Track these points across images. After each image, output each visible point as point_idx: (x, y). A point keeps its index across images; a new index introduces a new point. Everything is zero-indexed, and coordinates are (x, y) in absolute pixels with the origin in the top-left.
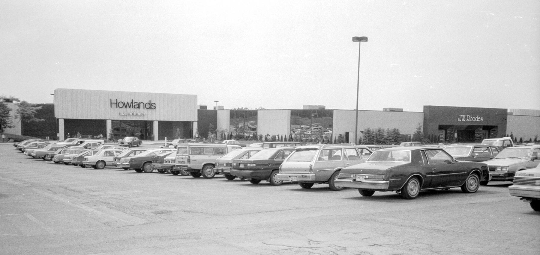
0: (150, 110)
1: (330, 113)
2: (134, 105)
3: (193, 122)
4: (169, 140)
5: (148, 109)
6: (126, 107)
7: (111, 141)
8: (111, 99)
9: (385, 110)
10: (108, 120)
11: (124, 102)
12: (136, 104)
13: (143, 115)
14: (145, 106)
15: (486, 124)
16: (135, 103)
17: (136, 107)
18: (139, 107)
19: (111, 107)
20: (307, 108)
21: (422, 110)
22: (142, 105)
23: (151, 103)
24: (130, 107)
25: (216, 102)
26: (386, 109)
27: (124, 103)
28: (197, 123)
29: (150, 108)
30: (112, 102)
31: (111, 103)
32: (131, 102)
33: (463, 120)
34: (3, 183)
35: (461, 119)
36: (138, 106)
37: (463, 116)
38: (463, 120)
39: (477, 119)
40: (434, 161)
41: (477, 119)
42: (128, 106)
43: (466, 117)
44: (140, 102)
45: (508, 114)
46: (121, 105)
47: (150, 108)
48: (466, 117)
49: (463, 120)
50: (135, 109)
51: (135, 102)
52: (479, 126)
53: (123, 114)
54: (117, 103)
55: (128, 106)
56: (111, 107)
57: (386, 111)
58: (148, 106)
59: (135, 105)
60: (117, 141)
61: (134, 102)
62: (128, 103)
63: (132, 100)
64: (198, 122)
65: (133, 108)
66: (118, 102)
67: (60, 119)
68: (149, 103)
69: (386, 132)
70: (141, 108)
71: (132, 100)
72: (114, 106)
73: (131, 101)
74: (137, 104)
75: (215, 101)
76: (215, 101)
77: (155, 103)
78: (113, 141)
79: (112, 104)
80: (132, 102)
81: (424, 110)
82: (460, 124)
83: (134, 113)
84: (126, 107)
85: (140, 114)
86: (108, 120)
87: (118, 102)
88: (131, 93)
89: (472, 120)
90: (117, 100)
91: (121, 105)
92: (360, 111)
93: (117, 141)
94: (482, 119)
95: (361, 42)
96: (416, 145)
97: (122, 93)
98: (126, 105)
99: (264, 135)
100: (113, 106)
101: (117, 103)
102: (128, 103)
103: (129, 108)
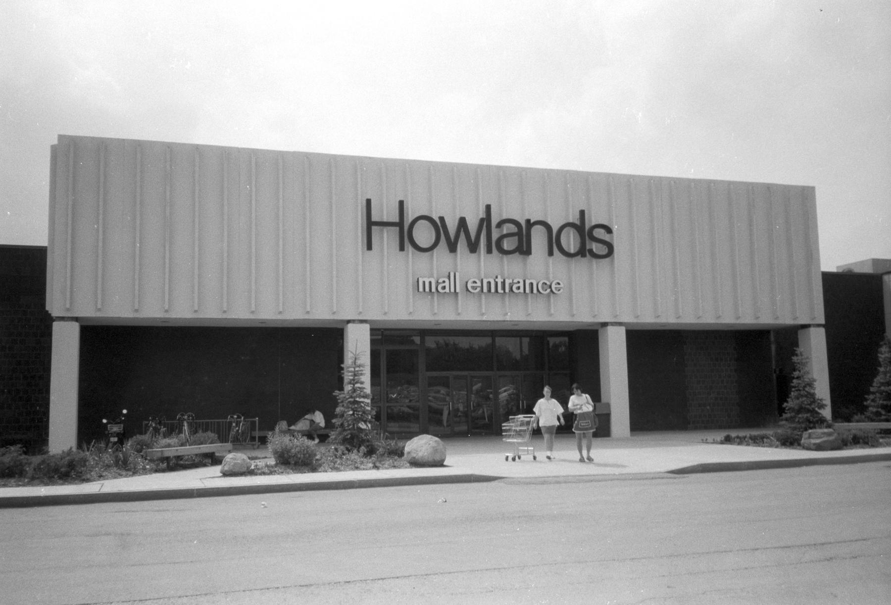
0: (581, 266)
2: (495, 235)
3: (801, 334)
4: (733, 434)
5: (574, 259)
6: (452, 248)
7: (354, 456)
8: (369, 202)
10: (353, 321)
11: (442, 219)
12: (508, 228)
13: (550, 291)
14: (554, 243)
16: (500, 225)
17: (507, 245)
18: (524, 249)
19: (369, 247)
22: (538, 239)
23: (587, 227)
24: (473, 247)
27: (439, 226)
28: (822, 331)
29: (584, 255)
30: (375, 218)
31: (370, 224)
32: (482, 220)
36: (520, 241)
40: (334, 485)
42: (462, 245)
44: (528, 221)
46: (424, 235)
47: (582, 252)
50: (505, 258)
51: (505, 217)
53: (437, 283)
54: (400, 224)
55: (462, 245)
56: (369, 247)
58: (570, 241)
59: (503, 237)
60: (400, 453)
61: (495, 221)
62: (462, 222)
63: (488, 208)
64: (830, 326)
65: (489, 251)
66: (409, 217)
67: (62, 323)
68: (578, 222)
70: (533, 250)
71: (488, 208)
72: (387, 239)
73: (482, 214)
74: (513, 228)
77: (605, 223)
78: (371, 452)
79: (375, 229)
80: (486, 221)
83: (499, 280)
84: (452, 248)
85: (532, 284)
86: (353, 321)
87: (409, 217)
88: (477, 173)
90: (401, 203)
91: (424, 235)
93: (400, 453)
96: (439, 462)
97: (430, 169)
98: (462, 236)
100: (382, 238)
101: (400, 224)
102: (462, 222)
103: (467, 250)
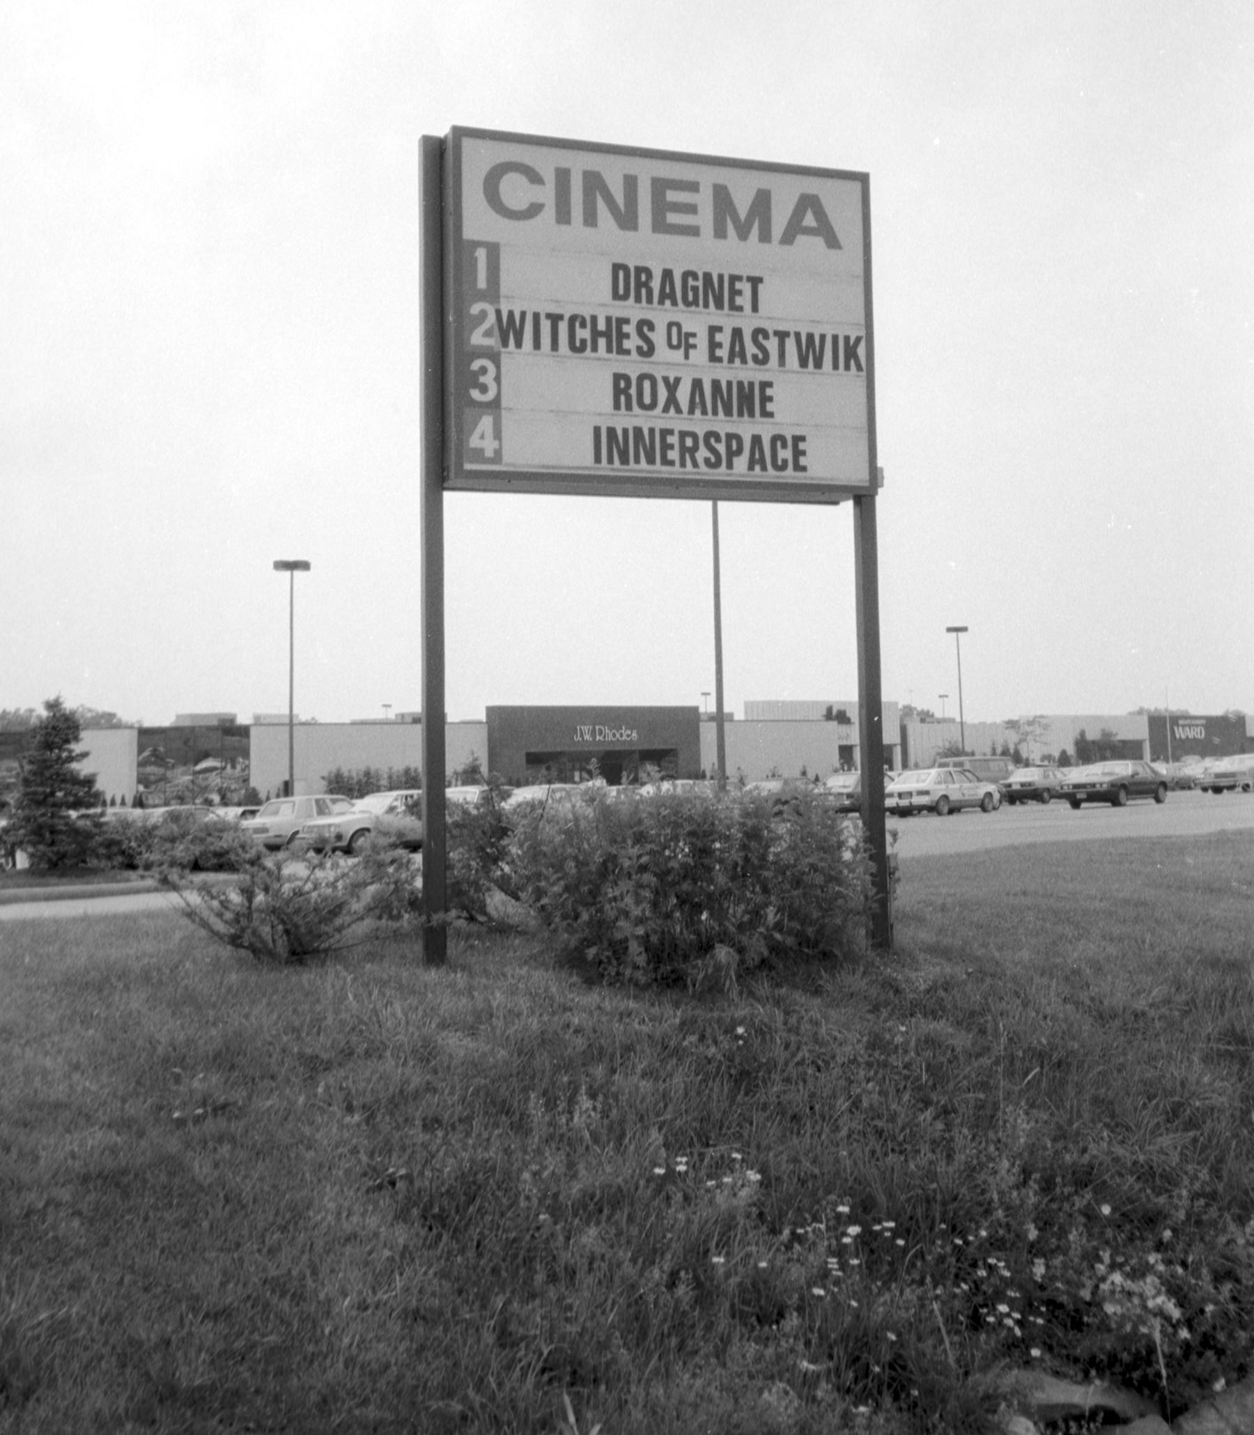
1: (244, 731)
9: (354, 724)
15: (646, 746)
20: (187, 723)
21: (482, 716)
25: (954, 634)
26: (403, 716)
33: (587, 737)
34: (117, 998)
35: (582, 735)
37: (586, 728)
38: (587, 737)
39: (621, 735)
41: (621, 735)
43: (594, 730)
45: (703, 717)
48: (594, 730)
49: (614, 737)
52: (631, 753)
57: (403, 723)
69: (385, 776)
75: (950, 630)
76: (950, 630)
81: (488, 716)
82: (580, 749)
89: (611, 738)
92: (302, 728)
94: (634, 734)
95: (722, 505)
99: (988, 751)
